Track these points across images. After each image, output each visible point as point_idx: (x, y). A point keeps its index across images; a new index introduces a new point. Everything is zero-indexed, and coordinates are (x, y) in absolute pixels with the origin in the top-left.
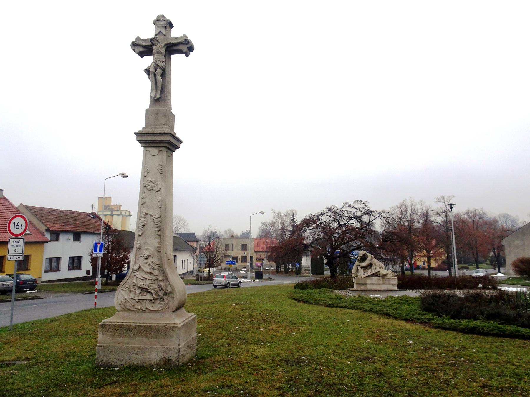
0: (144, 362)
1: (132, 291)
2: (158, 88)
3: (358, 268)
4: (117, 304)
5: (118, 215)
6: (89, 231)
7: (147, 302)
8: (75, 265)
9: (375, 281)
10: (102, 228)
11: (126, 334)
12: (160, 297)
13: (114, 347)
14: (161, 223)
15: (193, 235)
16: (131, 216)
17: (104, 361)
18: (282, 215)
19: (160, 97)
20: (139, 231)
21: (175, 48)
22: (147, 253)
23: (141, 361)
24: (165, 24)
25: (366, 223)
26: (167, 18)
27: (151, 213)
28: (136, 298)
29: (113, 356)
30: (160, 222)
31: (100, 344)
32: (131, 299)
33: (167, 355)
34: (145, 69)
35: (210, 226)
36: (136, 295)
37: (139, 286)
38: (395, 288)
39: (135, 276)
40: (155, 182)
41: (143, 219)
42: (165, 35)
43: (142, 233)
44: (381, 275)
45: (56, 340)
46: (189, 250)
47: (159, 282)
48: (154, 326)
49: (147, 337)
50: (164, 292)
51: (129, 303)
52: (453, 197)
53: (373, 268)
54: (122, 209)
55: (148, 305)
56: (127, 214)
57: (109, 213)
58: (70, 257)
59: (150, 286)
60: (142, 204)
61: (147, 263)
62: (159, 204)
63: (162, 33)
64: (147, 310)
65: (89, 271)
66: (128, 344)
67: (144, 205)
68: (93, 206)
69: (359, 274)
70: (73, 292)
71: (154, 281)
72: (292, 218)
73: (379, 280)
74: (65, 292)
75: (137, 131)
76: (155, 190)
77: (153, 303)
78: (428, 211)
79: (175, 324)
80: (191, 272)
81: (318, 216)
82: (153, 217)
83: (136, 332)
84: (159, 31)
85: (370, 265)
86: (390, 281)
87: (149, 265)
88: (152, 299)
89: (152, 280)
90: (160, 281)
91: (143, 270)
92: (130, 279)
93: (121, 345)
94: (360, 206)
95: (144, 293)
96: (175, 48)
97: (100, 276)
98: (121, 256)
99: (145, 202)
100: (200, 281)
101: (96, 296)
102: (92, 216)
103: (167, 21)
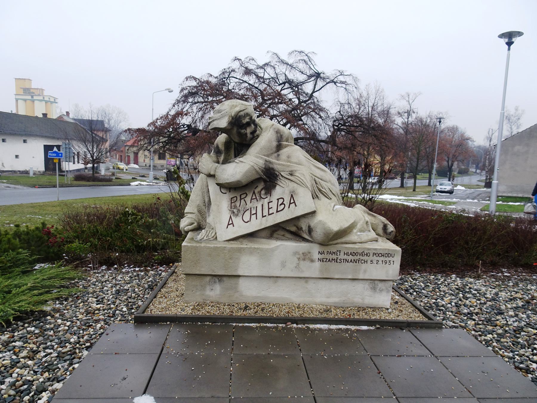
5: (41, 101)
9: (283, 265)
44: (318, 234)
53: (278, 192)
54: (45, 93)
56: (52, 100)
57: (30, 97)
73: (306, 257)
78: (389, 108)
86: (364, 266)
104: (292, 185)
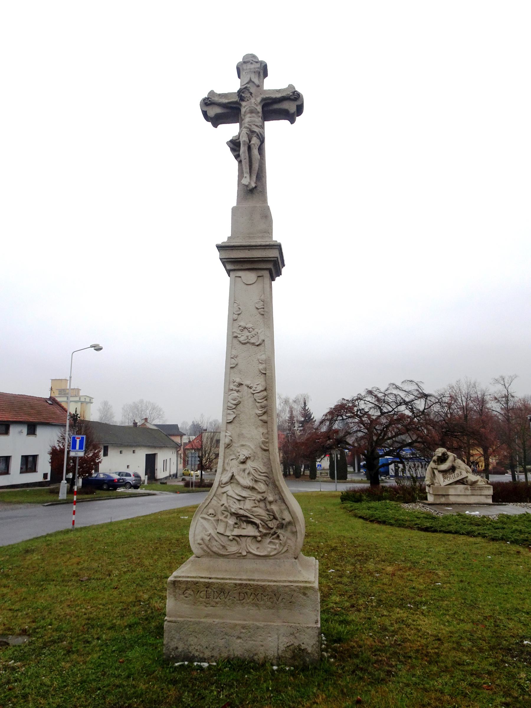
0: (255, 652)
1: (221, 520)
2: (253, 172)
3: (434, 473)
4: (194, 543)
6: (47, 421)
7: (249, 540)
8: (29, 466)
10: (68, 418)
11: (218, 600)
12: (272, 531)
13: (198, 623)
14: (266, 400)
15: (175, 427)
16: (92, 403)
17: (180, 650)
18: (291, 401)
19: (256, 187)
20: (229, 414)
21: (276, 106)
22: (244, 453)
23: (247, 651)
24: (258, 68)
25: (419, 410)
26: (260, 59)
27: (248, 382)
28: (228, 533)
29: (196, 640)
30: (266, 398)
31: (170, 617)
32: (219, 535)
33: (295, 641)
34: (229, 140)
35: (202, 415)
36: (228, 528)
37: (233, 510)
38: (490, 501)
39: (223, 493)
40: (253, 329)
41: (236, 394)
42: (258, 86)
43: (234, 418)
44: (469, 482)
45: (52, 590)
46: (172, 447)
47: (268, 504)
48: (269, 585)
49: (257, 605)
50: (278, 522)
51: (217, 541)
52: (516, 377)
53: (456, 472)
54: (81, 393)
55: (251, 545)
56: (88, 400)
58: (22, 456)
59: (252, 512)
60: (231, 368)
61: (244, 470)
62: (261, 367)
63: (253, 82)
64: (249, 555)
65: (47, 474)
66: (222, 618)
67: (235, 369)
68: (51, 389)
69: (437, 481)
70: (30, 503)
71: (259, 502)
72: (303, 405)
73: (467, 489)
74: (19, 503)
75: (220, 242)
76: (253, 344)
77: (259, 542)
78: (484, 395)
79: (306, 582)
80: (174, 475)
81: (353, 401)
82: (251, 391)
83: (236, 596)
84: (249, 79)
85: (453, 469)
87: (249, 473)
88: (258, 534)
89: (256, 502)
90: (271, 503)
91: (238, 483)
92: (215, 498)
93: (209, 620)
94: (412, 387)
95: (242, 523)
96: (276, 106)
97: (66, 482)
98: (91, 455)
99: (237, 365)
100: (190, 488)
101: (74, 511)
102: (50, 402)
103: (261, 64)
104: (460, 470)
